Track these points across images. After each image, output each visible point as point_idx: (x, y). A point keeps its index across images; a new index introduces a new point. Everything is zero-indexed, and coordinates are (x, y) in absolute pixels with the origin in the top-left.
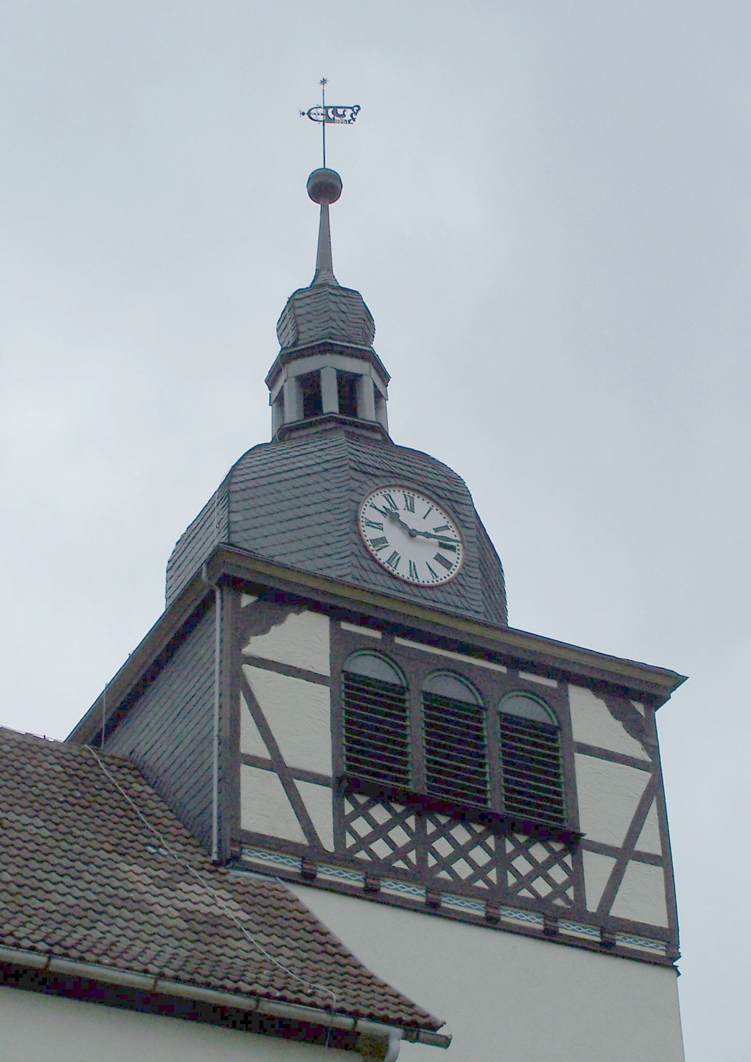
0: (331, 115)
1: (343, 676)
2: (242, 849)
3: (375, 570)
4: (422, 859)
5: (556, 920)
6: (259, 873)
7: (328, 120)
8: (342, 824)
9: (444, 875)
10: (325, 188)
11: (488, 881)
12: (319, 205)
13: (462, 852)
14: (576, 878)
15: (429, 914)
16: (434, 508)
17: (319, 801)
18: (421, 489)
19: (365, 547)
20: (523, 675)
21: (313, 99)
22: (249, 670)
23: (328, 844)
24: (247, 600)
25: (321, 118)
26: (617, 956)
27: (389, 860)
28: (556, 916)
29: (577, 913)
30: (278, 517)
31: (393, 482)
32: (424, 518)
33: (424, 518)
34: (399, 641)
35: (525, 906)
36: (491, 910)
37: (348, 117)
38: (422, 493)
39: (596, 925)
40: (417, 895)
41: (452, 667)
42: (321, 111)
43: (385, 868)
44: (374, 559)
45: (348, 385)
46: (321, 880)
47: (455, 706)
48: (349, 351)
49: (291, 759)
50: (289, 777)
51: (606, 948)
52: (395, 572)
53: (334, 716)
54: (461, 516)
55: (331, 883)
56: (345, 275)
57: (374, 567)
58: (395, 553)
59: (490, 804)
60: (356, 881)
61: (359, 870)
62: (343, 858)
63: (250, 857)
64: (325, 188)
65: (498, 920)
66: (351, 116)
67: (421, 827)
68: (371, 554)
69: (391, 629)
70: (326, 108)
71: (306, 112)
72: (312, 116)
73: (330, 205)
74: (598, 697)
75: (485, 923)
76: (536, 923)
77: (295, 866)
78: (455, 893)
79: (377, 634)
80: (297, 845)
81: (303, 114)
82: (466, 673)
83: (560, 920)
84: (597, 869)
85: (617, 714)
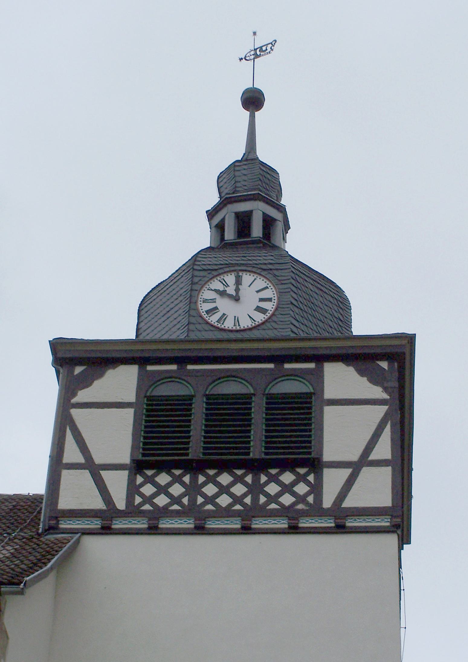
0: (258, 53)
1: (146, 399)
2: (58, 521)
3: (207, 329)
4: (193, 501)
5: (158, 519)
6: (68, 533)
7: (257, 56)
8: (133, 489)
9: (210, 507)
10: (253, 100)
11: (308, 504)
12: (248, 113)
13: (225, 489)
14: (317, 489)
15: (293, 533)
16: (258, 278)
17: (117, 484)
18: (249, 269)
19: (201, 317)
20: (287, 366)
21: (247, 47)
22: (74, 412)
23: (121, 505)
24: (78, 370)
25: (252, 57)
26: (254, 533)
27: (166, 507)
28: (296, 516)
29: (317, 510)
30: (159, 316)
31: (228, 269)
32: (249, 286)
33: (249, 286)
34: (190, 367)
35: (273, 514)
36: (339, 521)
37: (269, 49)
38: (246, 271)
39: (331, 516)
40: (188, 524)
41: (229, 374)
42: (253, 53)
43: (164, 512)
44: (207, 323)
45: (268, 223)
46: (162, 529)
47: (233, 399)
48: (233, 199)
49: (354, 457)
50: (95, 470)
51: (340, 529)
52: (242, 328)
53: (321, 429)
54: (278, 278)
55: (272, 529)
56: (264, 154)
57: (207, 327)
58: (224, 314)
59: (251, 455)
60: (142, 524)
61: (144, 517)
62: (133, 511)
63: (64, 525)
64: (253, 100)
65: (250, 528)
66: (271, 48)
67: (194, 479)
68: (205, 320)
69: (181, 361)
70: (255, 50)
71: (243, 57)
72: (247, 58)
73: (256, 113)
74: (348, 365)
75: (195, 532)
76: (283, 524)
77: (284, 523)
78: (215, 517)
79: (174, 367)
80: (100, 511)
81: (242, 59)
82: (174, 375)
83: (207, 519)
84: (333, 481)
85: (361, 373)
